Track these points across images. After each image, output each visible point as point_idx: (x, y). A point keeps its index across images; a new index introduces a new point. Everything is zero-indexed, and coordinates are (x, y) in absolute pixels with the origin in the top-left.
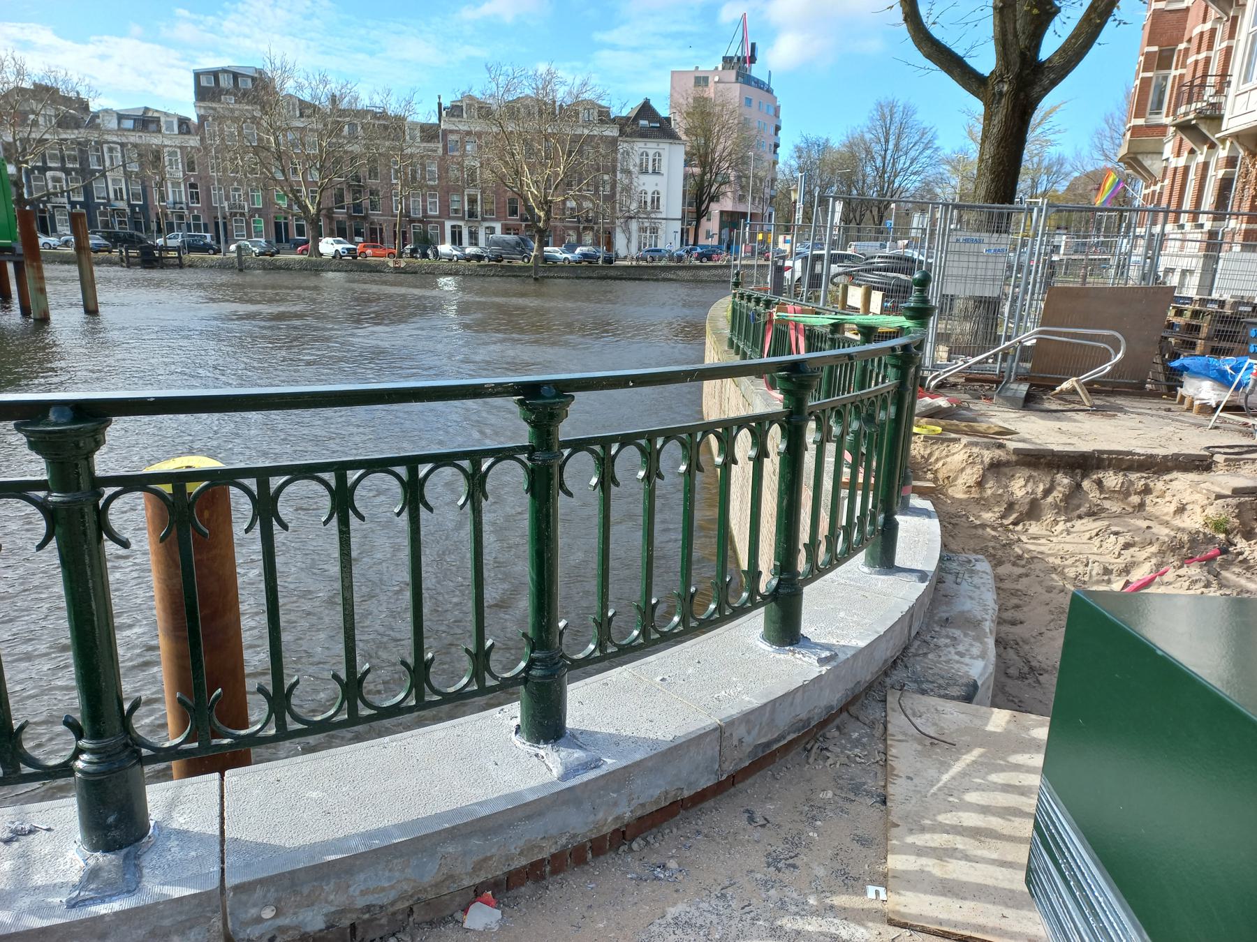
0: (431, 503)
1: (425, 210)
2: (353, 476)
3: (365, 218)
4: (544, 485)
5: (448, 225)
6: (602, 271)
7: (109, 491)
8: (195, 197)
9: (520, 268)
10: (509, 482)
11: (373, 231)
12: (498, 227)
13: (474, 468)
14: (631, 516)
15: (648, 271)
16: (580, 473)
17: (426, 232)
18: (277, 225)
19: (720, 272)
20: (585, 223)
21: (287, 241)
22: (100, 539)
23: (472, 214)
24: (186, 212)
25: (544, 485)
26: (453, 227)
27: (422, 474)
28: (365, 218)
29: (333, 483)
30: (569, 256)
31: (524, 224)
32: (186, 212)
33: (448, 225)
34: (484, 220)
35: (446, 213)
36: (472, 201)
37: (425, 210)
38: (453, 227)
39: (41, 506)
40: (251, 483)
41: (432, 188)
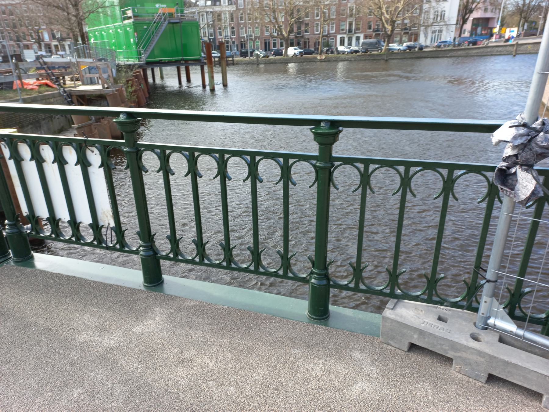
0: (457, 195)
1: (328, 31)
2: (291, 161)
3: (302, 37)
4: (325, 179)
5: (339, 37)
6: (416, 54)
7: (336, 163)
8: (233, 33)
9: (377, 55)
10: (303, 173)
11: (305, 43)
12: (362, 36)
13: (286, 162)
14: (184, 198)
15: (440, 52)
16: (345, 177)
17: (328, 41)
18: (265, 43)
19: (482, 50)
20: (406, 30)
21: (269, 50)
22: (329, 185)
23: (350, 31)
24: (230, 40)
25: (325, 179)
26: (341, 38)
27: (370, 170)
28: (302, 37)
29: (362, 170)
30: (401, 48)
31: (374, 34)
32: (230, 40)
33: (339, 37)
34: (355, 33)
35: (338, 32)
36: (351, 24)
37: (328, 31)
38: (341, 38)
39: (314, 166)
40: (402, 169)
41: (333, 19)
